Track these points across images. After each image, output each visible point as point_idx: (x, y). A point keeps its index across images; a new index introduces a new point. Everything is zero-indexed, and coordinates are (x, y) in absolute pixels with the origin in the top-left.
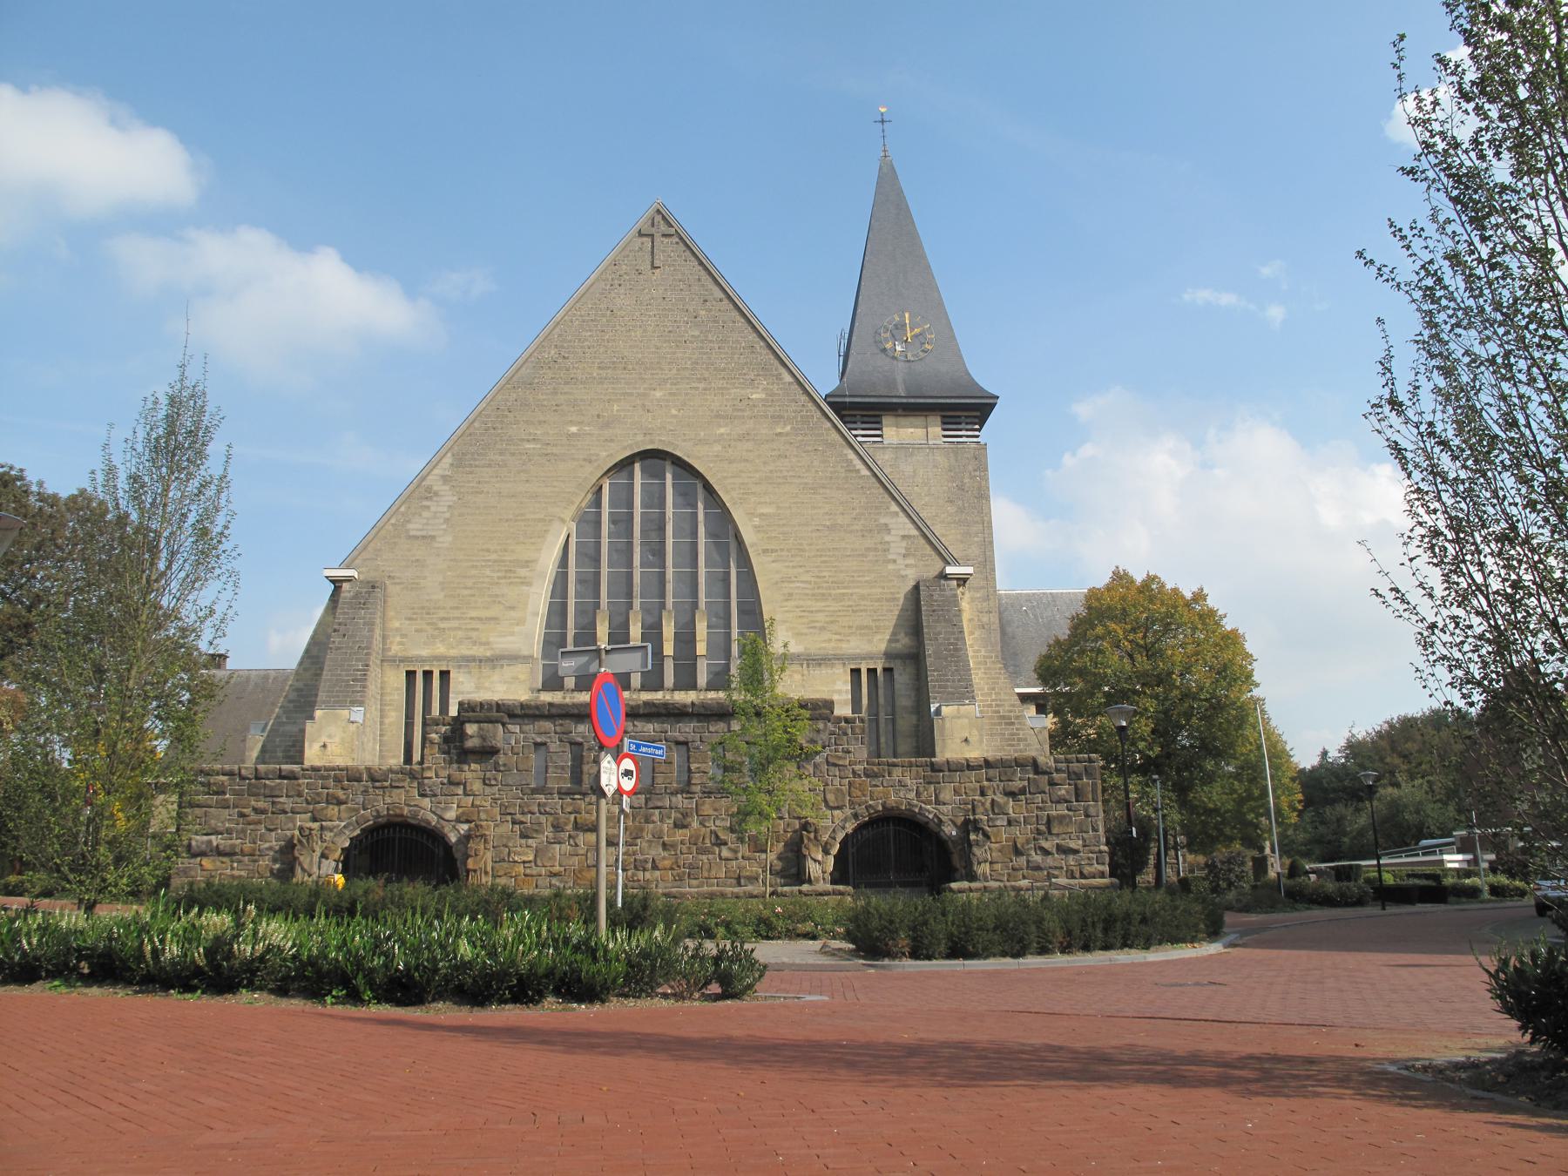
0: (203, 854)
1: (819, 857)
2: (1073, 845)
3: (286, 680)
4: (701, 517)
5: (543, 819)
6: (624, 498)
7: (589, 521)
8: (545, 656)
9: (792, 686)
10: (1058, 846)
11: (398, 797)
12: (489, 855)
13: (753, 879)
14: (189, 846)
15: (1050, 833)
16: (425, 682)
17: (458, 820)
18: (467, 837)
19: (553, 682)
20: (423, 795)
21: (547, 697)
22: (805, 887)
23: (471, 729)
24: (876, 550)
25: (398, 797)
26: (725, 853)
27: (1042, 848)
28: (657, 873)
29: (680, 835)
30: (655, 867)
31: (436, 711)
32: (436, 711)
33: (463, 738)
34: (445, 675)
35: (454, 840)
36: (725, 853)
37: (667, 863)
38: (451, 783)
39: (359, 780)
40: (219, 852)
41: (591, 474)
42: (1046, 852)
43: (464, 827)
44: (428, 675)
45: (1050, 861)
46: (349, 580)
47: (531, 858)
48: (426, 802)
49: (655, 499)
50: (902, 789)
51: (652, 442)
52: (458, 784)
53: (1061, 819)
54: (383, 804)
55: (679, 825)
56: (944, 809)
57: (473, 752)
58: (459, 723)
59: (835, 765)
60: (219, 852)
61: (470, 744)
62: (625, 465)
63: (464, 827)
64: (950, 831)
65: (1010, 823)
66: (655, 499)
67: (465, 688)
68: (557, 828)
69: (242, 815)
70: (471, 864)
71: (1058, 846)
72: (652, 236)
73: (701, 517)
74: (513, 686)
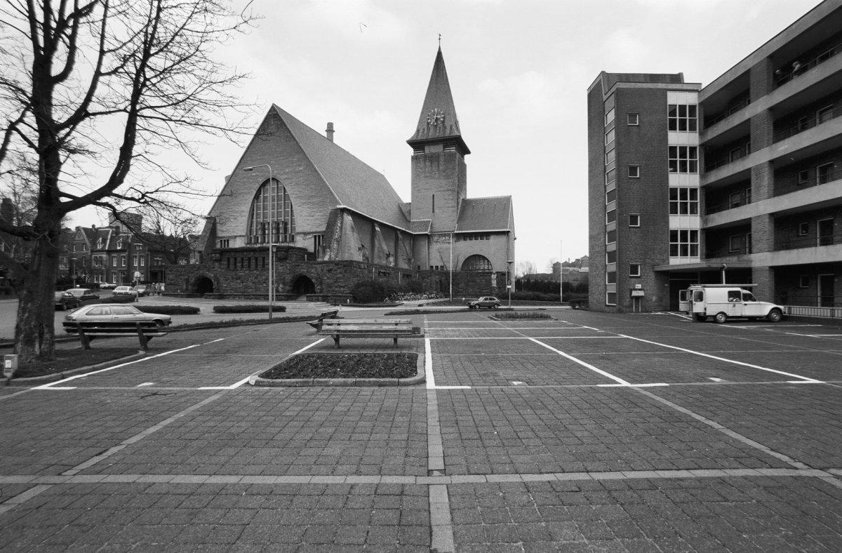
9: (300, 242)
19: (250, 242)
29: (257, 280)
34: (228, 241)
44: (225, 240)
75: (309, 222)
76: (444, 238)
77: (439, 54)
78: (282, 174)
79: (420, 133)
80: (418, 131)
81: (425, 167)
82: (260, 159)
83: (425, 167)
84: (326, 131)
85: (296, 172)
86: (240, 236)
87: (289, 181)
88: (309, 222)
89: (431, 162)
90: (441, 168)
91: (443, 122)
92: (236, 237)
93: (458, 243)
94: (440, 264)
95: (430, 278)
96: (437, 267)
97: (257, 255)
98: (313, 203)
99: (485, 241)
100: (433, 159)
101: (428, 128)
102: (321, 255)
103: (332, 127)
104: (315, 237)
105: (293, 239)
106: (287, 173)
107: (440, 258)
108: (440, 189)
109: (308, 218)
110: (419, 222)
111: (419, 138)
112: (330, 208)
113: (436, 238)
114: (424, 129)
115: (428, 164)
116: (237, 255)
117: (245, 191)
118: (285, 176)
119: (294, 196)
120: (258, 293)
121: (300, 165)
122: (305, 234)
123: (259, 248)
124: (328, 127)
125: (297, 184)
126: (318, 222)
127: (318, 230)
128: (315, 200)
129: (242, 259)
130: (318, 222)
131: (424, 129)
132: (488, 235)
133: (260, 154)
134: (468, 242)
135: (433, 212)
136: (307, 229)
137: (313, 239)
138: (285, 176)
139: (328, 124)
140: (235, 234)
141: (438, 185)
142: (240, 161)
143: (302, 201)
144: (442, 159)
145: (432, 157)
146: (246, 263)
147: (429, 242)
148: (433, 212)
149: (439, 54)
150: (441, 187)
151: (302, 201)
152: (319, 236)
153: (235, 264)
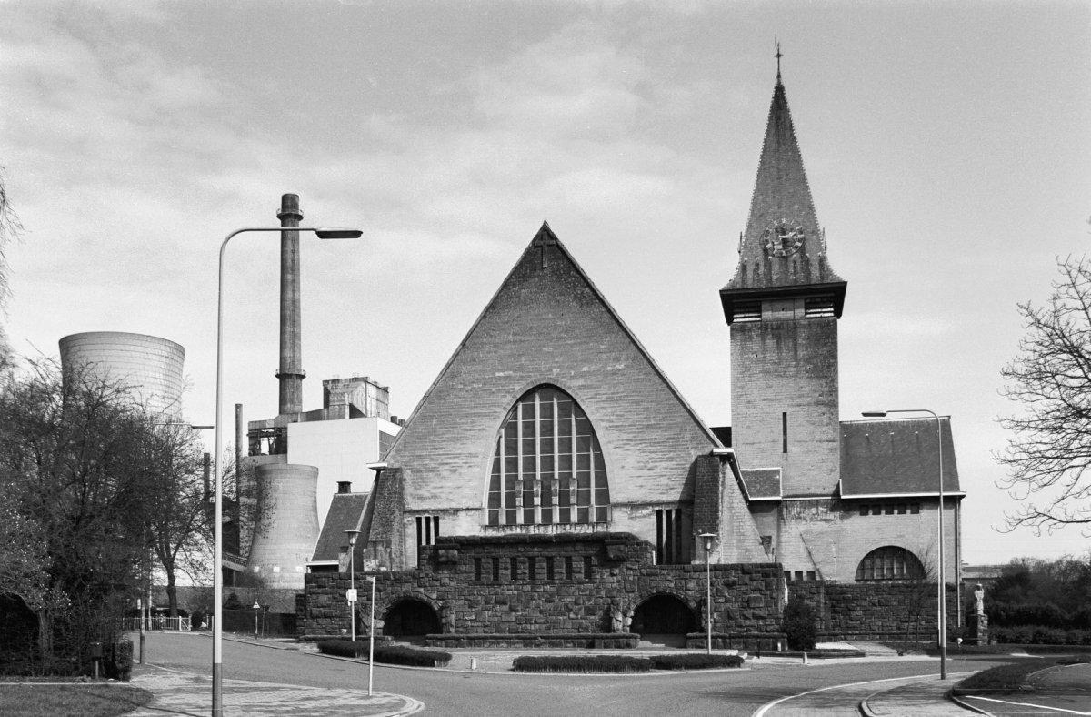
0: (317, 617)
1: (620, 618)
2: (762, 614)
3: (366, 496)
4: (573, 423)
5: (480, 598)
6: (529, 412)
7: (511, 428)
8: (490, 506)
9: (621, 523)
10: (753, 614)
11: (408, 587)
12: (453, 616)
13: (586, 629)
14: (311, 613)
15: (749, 606)
16: (429, 520)
17: (438, 599)
18: (442, 608)
19: (494, 522)
20: (419, 586)
21: (491, 533)
22: (612, 634)
23: (442, 552)
24: (673, 438)
25: (408, 587)
26: (572, 615)
27: (743, 615)
28: (537, 626)
29: (549, 606)
30: (536, 623)
31: (424, 543)
32: (424, 543)
33: (440, 553)
34: (436, 520)
35: (436, 609)
36: (572, 615)
37: (542, 621)
38: (434, 580)
39: (389, 579)
40: (326, 616)
41: (509, 400)
42: (746, 618)
43: (440, 603)
44: (428, 519)
45: (748, 623)
46: (384, 469)
47: (474, 617)
48: (422, 590)
49: (547, 411)
50: (668, 582)
51: (545, 378)
52: (437, 580)
53: (756, 599)
54: (408, 588)
55: (548, 601)
56: (690, 592)
57: (442, 563)
58: (436, 548)
59: (631, 569)
60: (326, 616)
61: (443, 559)
62: (528, 396)
63: (440, 603)
64: (693, 605)
65: (726, 601)
66: (547, 411)
67: (449, 528)
68: (486, 603)
69: (335, 598)
70: (443, 621)
71: (753, 614)
72: (541, 246)
73: (573, 423)
74: (466, 527)
75: (640, 482)
76: (814, 510)
77: (779, 90)
78: (572, 378)
79: (750, 274)
80: (744, 267)
81: (764, 350)
82: (515, 342)
83: (764, 350)
84: (279, 217)
85: (606, 375)
86: (468, 509)
87: (592, 392)
88: (640, 482)
89: (778, 338)
90: (802, 353)
91: (802, 250)
92: (456, 511)
93: (846, 521)
94: (805, 567)
95: (816, 597)
96: (799, 573)
97: (551, 552)
98: (653, 442)
99: (908, 517)
100: (781, 332)
101: (768, 264)
102: (699, 551)
103: (296, 206)
104: (659, 513)
105: (603, 518)
106: (583, 375)
107: (806, 554)
108: (799, 401)
109: (640, 473)
110: (753, 473)
111: (750, 284)
112: (694, 454)
113: (795, 510)
114: (757, 265)
115: (770, 343)
116: (500, 552)
117: (476, 410)
118: (581, 382)
119: (603, 424)
120: (553, 633)
121: (617, 359)
122: (634, 506)
123: (557, 536)
124: (284, 206)
125: (609, 400)
126: (664, 481)
127: (665, 498)
128: (655, 435)
129: (514, 560)
130: (664, 481)
131: (757, 265)
132: (915, 505)
133: (517, 329)
134: (871, 519)
135: (785, 451)
136: (638, 496)
137: (654, 518)
138: (581, 382)
139: (285, 198)
140: (454, 505)
141: (786, 392)
142: (464, 344)
143: (625, 436)
144: (803, 334)
145: (778, 328)
146: (524, 569)
147: (780, 517)
148: (785, 451)
149: (779, 90)
150: (800, 396)
151: (625, 436)
152: (669, 512)
153: (496, 569)
